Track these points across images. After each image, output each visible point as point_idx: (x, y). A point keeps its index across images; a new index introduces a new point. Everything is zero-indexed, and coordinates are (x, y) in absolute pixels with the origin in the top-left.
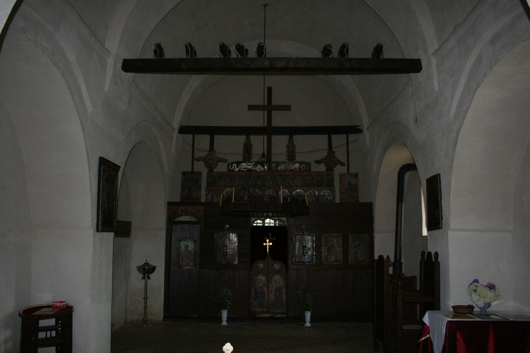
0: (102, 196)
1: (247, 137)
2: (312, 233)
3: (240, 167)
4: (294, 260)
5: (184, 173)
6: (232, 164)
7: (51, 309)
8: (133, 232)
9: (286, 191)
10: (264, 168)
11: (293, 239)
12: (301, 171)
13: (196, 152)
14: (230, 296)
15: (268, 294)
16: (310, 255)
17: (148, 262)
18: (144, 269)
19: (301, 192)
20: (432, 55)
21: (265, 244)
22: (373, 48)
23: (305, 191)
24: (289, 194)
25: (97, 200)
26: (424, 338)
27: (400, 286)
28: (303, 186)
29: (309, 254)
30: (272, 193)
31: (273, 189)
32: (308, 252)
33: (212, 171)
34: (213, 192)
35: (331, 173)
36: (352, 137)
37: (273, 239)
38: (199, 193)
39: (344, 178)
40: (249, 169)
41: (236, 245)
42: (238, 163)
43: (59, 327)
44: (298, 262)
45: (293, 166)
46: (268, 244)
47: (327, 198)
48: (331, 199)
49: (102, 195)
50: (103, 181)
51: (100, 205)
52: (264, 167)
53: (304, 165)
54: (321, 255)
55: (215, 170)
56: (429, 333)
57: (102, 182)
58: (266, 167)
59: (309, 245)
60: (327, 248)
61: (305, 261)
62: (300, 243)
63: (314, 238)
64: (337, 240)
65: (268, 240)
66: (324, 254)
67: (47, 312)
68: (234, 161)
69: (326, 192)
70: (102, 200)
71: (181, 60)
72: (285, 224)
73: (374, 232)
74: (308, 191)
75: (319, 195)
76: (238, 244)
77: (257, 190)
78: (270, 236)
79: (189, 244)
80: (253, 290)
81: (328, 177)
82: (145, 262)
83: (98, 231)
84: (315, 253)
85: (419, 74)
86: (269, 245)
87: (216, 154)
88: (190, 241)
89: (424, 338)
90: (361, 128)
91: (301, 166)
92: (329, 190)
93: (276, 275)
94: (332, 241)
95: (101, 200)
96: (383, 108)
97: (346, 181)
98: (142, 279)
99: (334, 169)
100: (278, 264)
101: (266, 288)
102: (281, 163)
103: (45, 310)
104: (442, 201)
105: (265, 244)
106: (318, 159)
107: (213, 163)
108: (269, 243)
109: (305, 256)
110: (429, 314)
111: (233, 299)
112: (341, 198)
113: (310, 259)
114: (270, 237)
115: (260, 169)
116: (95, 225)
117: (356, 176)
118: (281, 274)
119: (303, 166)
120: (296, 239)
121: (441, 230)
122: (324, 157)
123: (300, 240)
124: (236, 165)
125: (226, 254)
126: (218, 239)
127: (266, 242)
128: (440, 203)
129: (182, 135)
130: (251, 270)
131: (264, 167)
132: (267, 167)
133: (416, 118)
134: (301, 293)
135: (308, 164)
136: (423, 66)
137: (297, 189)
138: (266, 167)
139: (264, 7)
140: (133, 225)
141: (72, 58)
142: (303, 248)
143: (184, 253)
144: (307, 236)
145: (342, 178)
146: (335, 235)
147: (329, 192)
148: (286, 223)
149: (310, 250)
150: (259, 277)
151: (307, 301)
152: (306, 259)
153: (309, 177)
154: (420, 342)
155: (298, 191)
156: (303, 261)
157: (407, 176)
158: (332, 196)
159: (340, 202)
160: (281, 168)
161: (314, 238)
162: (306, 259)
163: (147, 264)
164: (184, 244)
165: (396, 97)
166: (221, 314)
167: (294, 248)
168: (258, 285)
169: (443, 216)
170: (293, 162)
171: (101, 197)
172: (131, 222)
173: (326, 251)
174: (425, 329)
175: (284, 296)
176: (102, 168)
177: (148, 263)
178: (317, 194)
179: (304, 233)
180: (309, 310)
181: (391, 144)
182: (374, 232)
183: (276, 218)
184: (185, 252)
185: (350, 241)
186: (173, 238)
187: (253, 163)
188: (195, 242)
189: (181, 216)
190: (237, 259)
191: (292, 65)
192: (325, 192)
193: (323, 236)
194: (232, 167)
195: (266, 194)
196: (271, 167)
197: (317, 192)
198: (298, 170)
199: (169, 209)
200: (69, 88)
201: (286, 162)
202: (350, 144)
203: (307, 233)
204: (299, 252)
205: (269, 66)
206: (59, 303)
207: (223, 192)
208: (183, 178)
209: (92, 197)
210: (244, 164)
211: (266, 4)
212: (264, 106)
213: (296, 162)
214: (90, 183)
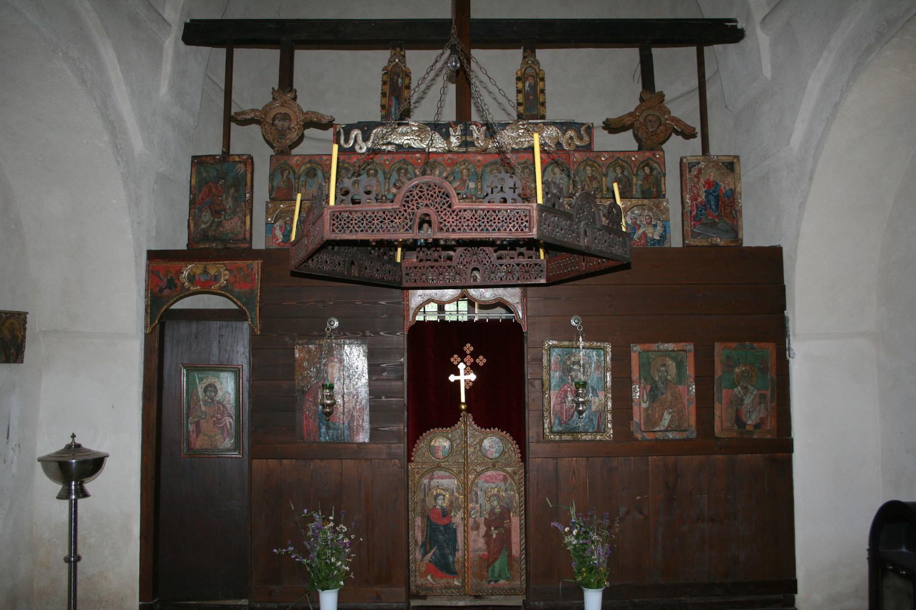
4: (546, 426)
5: (198, 162)
6: (348, 129)
11: (541, 360)
14: (345, 547)
21: (452, 378)
35: (654, 155)
36: (713, 52)
37: (477, 361)
38: (245, 223)
46: (464, 377)
47: (644, 234)
76: (370, 379)
78: (468, 352)
81: (647, 170)
97: (702, 181)
101: (460, 515)
105: (452, 378)
114: (468, 357)
117: (730, 166)
124: (359, 132)
126: (305, 364)
127: (457, 373)
130: (412, 459)
158: (659, 228)
163: (74, 448)
177: (79, 446)
182: (791, 338)
194: (347, 141)
198: (553, 146)
208: (194, 176)
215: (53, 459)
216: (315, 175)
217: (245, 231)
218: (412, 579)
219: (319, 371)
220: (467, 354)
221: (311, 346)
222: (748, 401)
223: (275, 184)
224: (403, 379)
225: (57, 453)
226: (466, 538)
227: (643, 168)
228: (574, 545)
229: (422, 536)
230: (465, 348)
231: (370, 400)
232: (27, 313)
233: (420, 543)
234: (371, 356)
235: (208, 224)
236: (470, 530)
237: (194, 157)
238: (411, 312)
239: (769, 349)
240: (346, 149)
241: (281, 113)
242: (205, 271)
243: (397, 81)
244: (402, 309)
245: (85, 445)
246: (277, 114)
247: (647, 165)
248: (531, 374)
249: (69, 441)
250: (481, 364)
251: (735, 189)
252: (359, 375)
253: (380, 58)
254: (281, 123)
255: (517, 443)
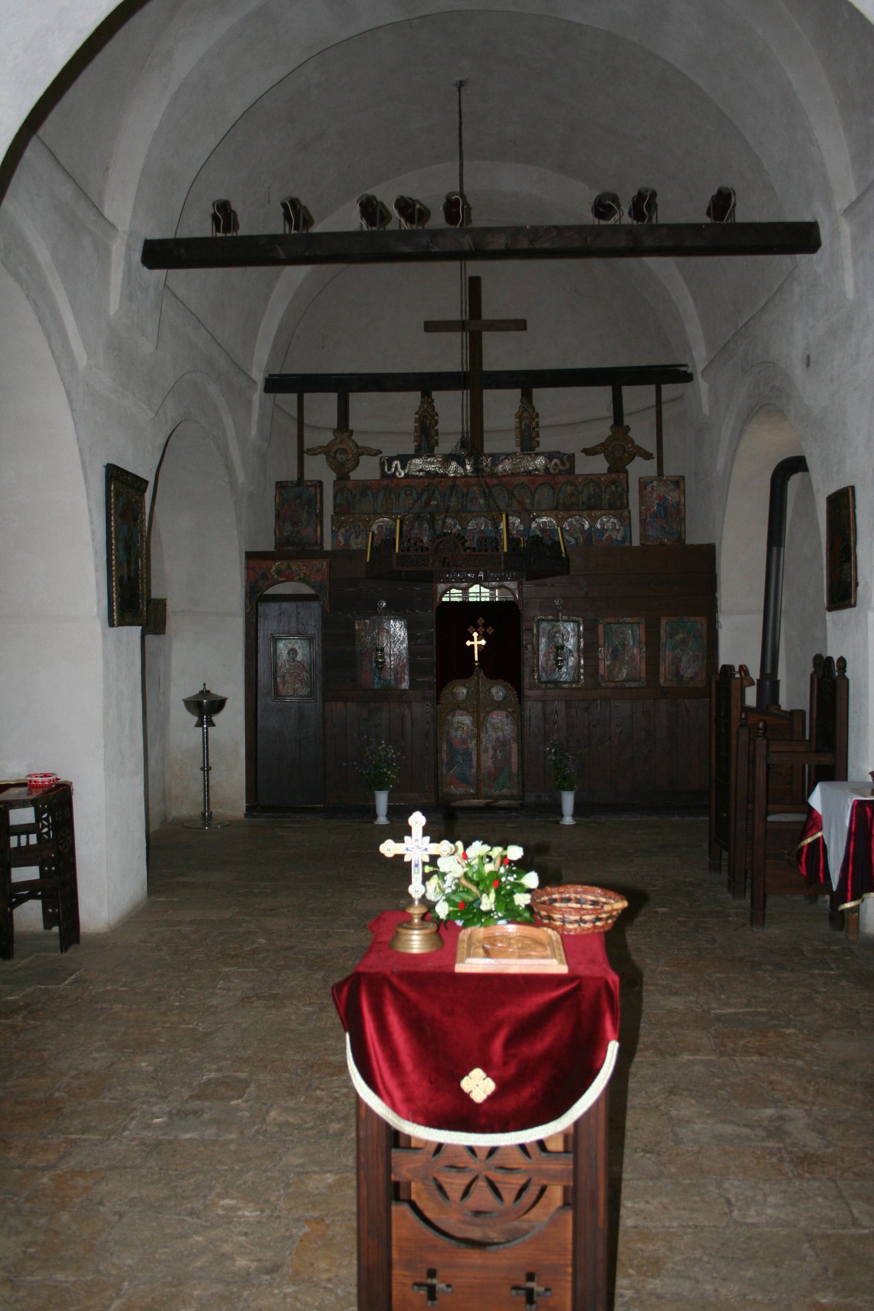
0: (117, 549)
1: (423, 396)
2: (576, 616)
3: (409, 468)
4: (536, 677)
5: (281, 486)
6: (391, 460)
7: (25, 789)
8: (172, 623)
9: (517, 522)
10: (465, 469)
11: (532, 630)
12: (550, 473)
13: (307, 433)
14: (393, 761)
15: (478, 754)
16: (572, 667)
17: (208, 688)
18: (199, 704)
19: (550, 522)
20: (842, 215)
21: (468, 643)
22: (709, 198)
23: (560, 521)
24: (522, 529)
25: (105, 558)
26: (809, 840)
27: (761, 731)
28: (556, 509)
29: (570, 664)
30: (485, 527)
31: (485, 517)
32: (568, 659)
33: (348, 478)
34: (348, 528)
35: (619, 476)
36: (669, 391)
37: (488, 630)
38: (316, 531)
39: (649, 489)
40: (429, 472)
41: (405, 645)
42: (405, 459)
43: (44, 826)
44: (546, 683)
45: (532, 463)
46: (477, 642)
47: (610, 536)
48: (619, 539)
49: (115, 546)
50: (117, 517)
51: (114, 568)
52: (463, 465)
53: (555, 461)
54: (597, 666)
55: (354, 476)
56: (821, 829)
57: (115, 518)
58: (468, 467)
59: (571, 643)
60: (611, 649)
61: (562, 680)
62: (548, 638)
63: (581, 628)
64: (632, 632)
65: (475, 635)
66: (604, 663)
67: (22, 796)
68: (395, 454)
69: (608, 522)
70: (116, 557)
71: (273, 239)
72: (515, 596)
73: (717, 612)
74: (566, 520)
75: (593, 528)
76: (409, 645)
77: (449, 521)
78: (480, 624)
79: (296, 647)
80: (445, 747)
81: (613, 487)
82: (202, 689)
83: (111, 624)
84: (582, 662)
85: (814, 257)
86: (478, 645)
87: (354, 437)
88: (300, 639)
89: (809, 840)
90: (690, 370)
91: (551, 461)
92: (615, 517)
93: (495, 712)
94: (622, 634)
95: (113, 557)
96: (739, 327)
97: (655, 495)
98: (197, 726)
99: (628, 467)
100: (499, 687)
101: (474, 742)
102: (503, 457)
103: (17, 790)
104: (858, 546)
105: (468, 643)
106: (589, 445)
107: (347, 460)
108: (478, 640)
109: (560, 668)
110: (822, 790)
111: (399, 768)
112: (643, 536)
113: (572, 676)
114: (481, 627)
115: (455, 472)
116: (106, 612)
117: (678, 482)
118: (506, 711)
119: (553, 463)
120: (541, 630)
121: (854, 608)
122: (602, 440)
123: (549, 632)
124: (399, 462)
125: (382, 668)
126: (363, 634)
127: (472, 639)
128: (852, 551)
129: (272, 395)
130: (440, 702)
131: (463, 465)
132: (471, 467)
133: (808, 357)
134: (553, 751)
135: (565, 457)
136: (822, 238)
137: (540, 517)
138: (468, 467)
139: (456, 89)
140: (170, 607)
141: (43, 254)
142: (555, 650)
143: (287, 666)
144: (565, 624)
145: (645, 489)
146: (628, 620)
147: (614, 522)
148: (517, 595)
149: (573, 656)
150: (457, 717)
151: (567, 769)
152: (565, 674)
153: (569, 487)
154: (803, 847)
155: (545, 519)
156: (557, 679)
157: (794, 482)
158: (621, 532)
159: (641, 543)
160: (502, 467)
161: (581, 628)
162: (565, 674)
163: (205, 693)
164: (285, 645)
165: (767, 303)
166: (373, 799)
167: (536, 651)
168: (456, 736)
169: (860, 579)
170: (530, 455)
171: (113, 552)
172: (166, 599)
173: (608, 655)
174: (813, 821)
175: (515, 760)
176: (112, 489)
177: (208, 692)
178: (587, 526)
179: (558, 616)
180: (571, 790)
181: (756, 412)
182: (719, 613)
183: (494, 583)
184: (289, 664)
185: (663, 634)
186: (261, 635)
187: (439, 458)
188: (310, 640)
189: (277, 582)
190: (406, 677)
191: (524, 244)
192: (607, 522)
193: (601, 624)
194: (389, 469)
195: (469, 528)
196: (481, 467)
197: (587, 522)
198: (543, 471)
199: (248, 568)
200: (40, 322)
201: (515, 453)
202: (664, 407)
203: (565, 617)
204: (547, 660)
205: (473, 247)
206: (41, 777)
207: (371, 526)
208: (277, 496)
209: (96, 553)
210: (417, 461)
211: (461, 82)
212: (463, 322)
213: (538, 455)
214: (92, 523)
215: (193, 700)
216: (367, 495)
217: (317, 537)
218: (439, 788)
219: (373, 639)
220: (479, 626)
221: (366, 621)
222: (684, 659)
223: (338, 502)
224: (432, 643)
225: (195, 696)
226: (479, 759)
227: (610, 486)
228: (554, 761)
229: (447, 758)
230: (478, 621)
231: (409, 660)
232: (166, 599)
233: (446, 762)
234: (410, 628)
235: (290, 533)
236: (481, 753)
237: (277, 483)
238: (439, 596)
239: (699, 624)
240: (389, 475)
241: (340, 449)
242: (289, 567)
243: (426, 423)
244: (432, 596)
245: (213, 691)
246: (338, 449)
247: (613, 484)
248: (525, 640)
249: (202, 689)
250: (490, 633)
251: (680, 501)
252: (402, 641)
253: (414, 398)
254: (340, 457)
255: (515, 690)
